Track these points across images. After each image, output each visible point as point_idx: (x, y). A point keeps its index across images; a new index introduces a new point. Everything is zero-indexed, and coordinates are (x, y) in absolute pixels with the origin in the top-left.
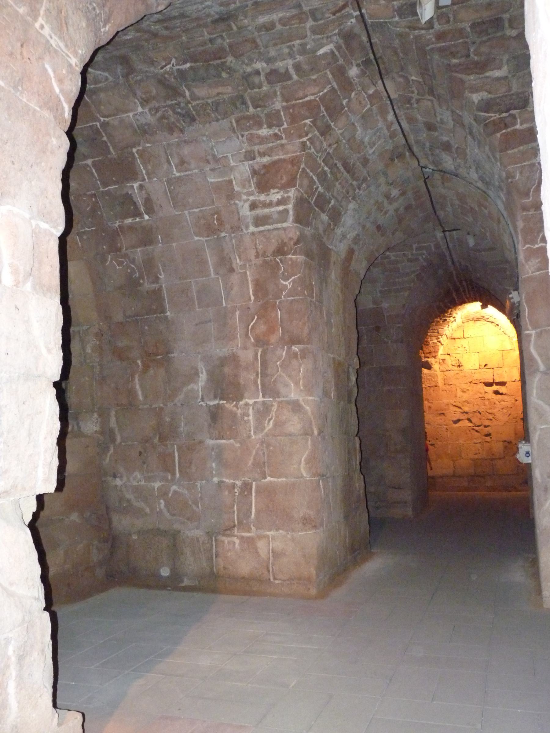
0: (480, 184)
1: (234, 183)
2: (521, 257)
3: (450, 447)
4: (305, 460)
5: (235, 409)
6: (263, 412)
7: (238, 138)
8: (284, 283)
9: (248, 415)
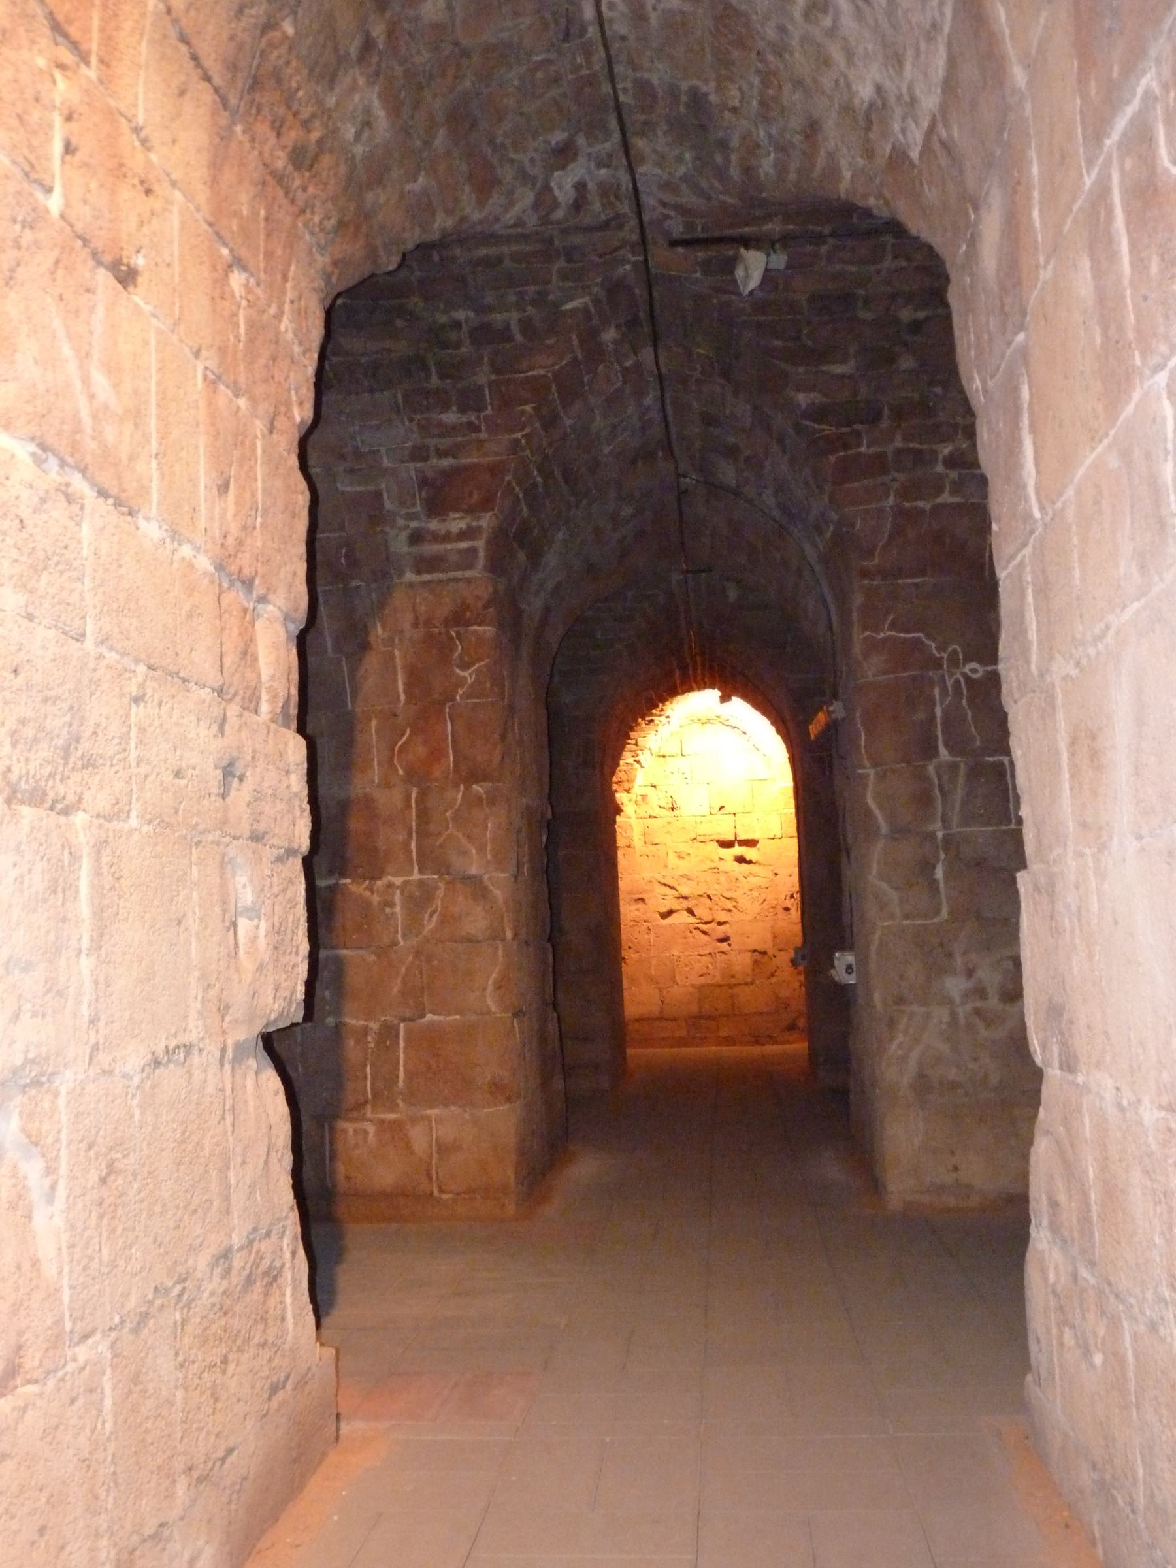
0: (776, 513)
1: (385, 496)
2: (857, 649)
3: (654, 962)
4: (494, 983)
5: (367, 894)
6: (419, 900)
7: (403, 423)
8: (462, 673)
9: (392, 904)
